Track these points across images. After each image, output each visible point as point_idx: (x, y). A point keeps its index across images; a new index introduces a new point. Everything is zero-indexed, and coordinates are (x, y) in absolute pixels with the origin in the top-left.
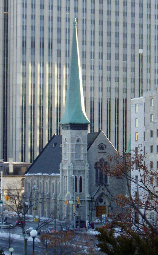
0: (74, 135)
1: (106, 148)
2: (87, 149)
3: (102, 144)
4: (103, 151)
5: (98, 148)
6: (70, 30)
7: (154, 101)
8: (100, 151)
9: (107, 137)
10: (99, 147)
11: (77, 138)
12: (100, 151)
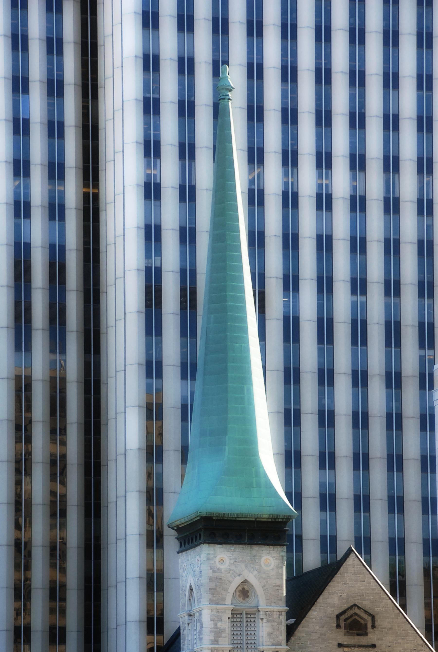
0: (223, 567)
1: (373, 626)
2: (283, 629)
3: (356, 610)
4: (363, 640)
5: (338, 626)
6: (407, 546)
7: (283, 594)
8: (345, 640)
9: (393, 593)
10: (342, 624)
11: (238, 581)
12: (345, 640)
